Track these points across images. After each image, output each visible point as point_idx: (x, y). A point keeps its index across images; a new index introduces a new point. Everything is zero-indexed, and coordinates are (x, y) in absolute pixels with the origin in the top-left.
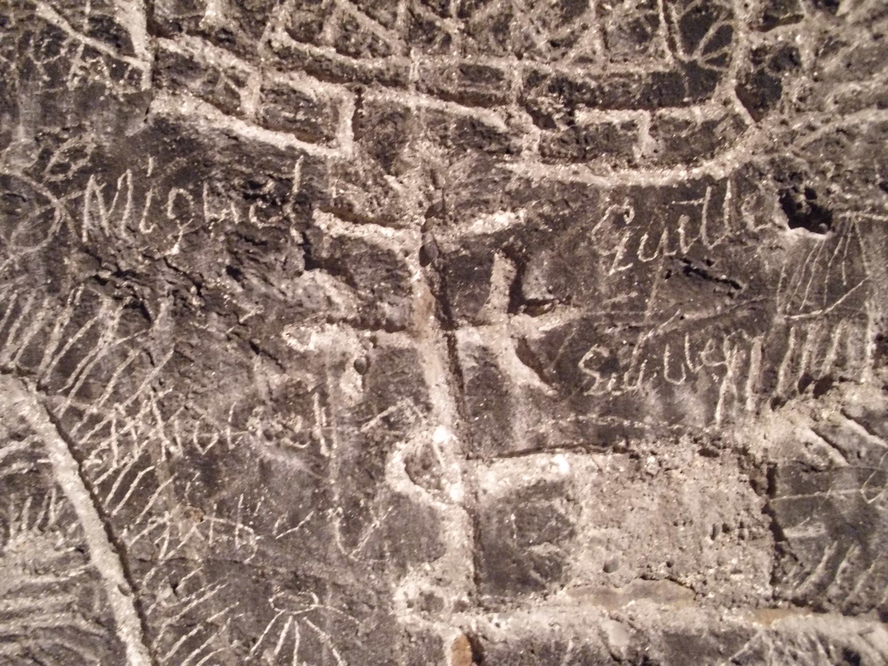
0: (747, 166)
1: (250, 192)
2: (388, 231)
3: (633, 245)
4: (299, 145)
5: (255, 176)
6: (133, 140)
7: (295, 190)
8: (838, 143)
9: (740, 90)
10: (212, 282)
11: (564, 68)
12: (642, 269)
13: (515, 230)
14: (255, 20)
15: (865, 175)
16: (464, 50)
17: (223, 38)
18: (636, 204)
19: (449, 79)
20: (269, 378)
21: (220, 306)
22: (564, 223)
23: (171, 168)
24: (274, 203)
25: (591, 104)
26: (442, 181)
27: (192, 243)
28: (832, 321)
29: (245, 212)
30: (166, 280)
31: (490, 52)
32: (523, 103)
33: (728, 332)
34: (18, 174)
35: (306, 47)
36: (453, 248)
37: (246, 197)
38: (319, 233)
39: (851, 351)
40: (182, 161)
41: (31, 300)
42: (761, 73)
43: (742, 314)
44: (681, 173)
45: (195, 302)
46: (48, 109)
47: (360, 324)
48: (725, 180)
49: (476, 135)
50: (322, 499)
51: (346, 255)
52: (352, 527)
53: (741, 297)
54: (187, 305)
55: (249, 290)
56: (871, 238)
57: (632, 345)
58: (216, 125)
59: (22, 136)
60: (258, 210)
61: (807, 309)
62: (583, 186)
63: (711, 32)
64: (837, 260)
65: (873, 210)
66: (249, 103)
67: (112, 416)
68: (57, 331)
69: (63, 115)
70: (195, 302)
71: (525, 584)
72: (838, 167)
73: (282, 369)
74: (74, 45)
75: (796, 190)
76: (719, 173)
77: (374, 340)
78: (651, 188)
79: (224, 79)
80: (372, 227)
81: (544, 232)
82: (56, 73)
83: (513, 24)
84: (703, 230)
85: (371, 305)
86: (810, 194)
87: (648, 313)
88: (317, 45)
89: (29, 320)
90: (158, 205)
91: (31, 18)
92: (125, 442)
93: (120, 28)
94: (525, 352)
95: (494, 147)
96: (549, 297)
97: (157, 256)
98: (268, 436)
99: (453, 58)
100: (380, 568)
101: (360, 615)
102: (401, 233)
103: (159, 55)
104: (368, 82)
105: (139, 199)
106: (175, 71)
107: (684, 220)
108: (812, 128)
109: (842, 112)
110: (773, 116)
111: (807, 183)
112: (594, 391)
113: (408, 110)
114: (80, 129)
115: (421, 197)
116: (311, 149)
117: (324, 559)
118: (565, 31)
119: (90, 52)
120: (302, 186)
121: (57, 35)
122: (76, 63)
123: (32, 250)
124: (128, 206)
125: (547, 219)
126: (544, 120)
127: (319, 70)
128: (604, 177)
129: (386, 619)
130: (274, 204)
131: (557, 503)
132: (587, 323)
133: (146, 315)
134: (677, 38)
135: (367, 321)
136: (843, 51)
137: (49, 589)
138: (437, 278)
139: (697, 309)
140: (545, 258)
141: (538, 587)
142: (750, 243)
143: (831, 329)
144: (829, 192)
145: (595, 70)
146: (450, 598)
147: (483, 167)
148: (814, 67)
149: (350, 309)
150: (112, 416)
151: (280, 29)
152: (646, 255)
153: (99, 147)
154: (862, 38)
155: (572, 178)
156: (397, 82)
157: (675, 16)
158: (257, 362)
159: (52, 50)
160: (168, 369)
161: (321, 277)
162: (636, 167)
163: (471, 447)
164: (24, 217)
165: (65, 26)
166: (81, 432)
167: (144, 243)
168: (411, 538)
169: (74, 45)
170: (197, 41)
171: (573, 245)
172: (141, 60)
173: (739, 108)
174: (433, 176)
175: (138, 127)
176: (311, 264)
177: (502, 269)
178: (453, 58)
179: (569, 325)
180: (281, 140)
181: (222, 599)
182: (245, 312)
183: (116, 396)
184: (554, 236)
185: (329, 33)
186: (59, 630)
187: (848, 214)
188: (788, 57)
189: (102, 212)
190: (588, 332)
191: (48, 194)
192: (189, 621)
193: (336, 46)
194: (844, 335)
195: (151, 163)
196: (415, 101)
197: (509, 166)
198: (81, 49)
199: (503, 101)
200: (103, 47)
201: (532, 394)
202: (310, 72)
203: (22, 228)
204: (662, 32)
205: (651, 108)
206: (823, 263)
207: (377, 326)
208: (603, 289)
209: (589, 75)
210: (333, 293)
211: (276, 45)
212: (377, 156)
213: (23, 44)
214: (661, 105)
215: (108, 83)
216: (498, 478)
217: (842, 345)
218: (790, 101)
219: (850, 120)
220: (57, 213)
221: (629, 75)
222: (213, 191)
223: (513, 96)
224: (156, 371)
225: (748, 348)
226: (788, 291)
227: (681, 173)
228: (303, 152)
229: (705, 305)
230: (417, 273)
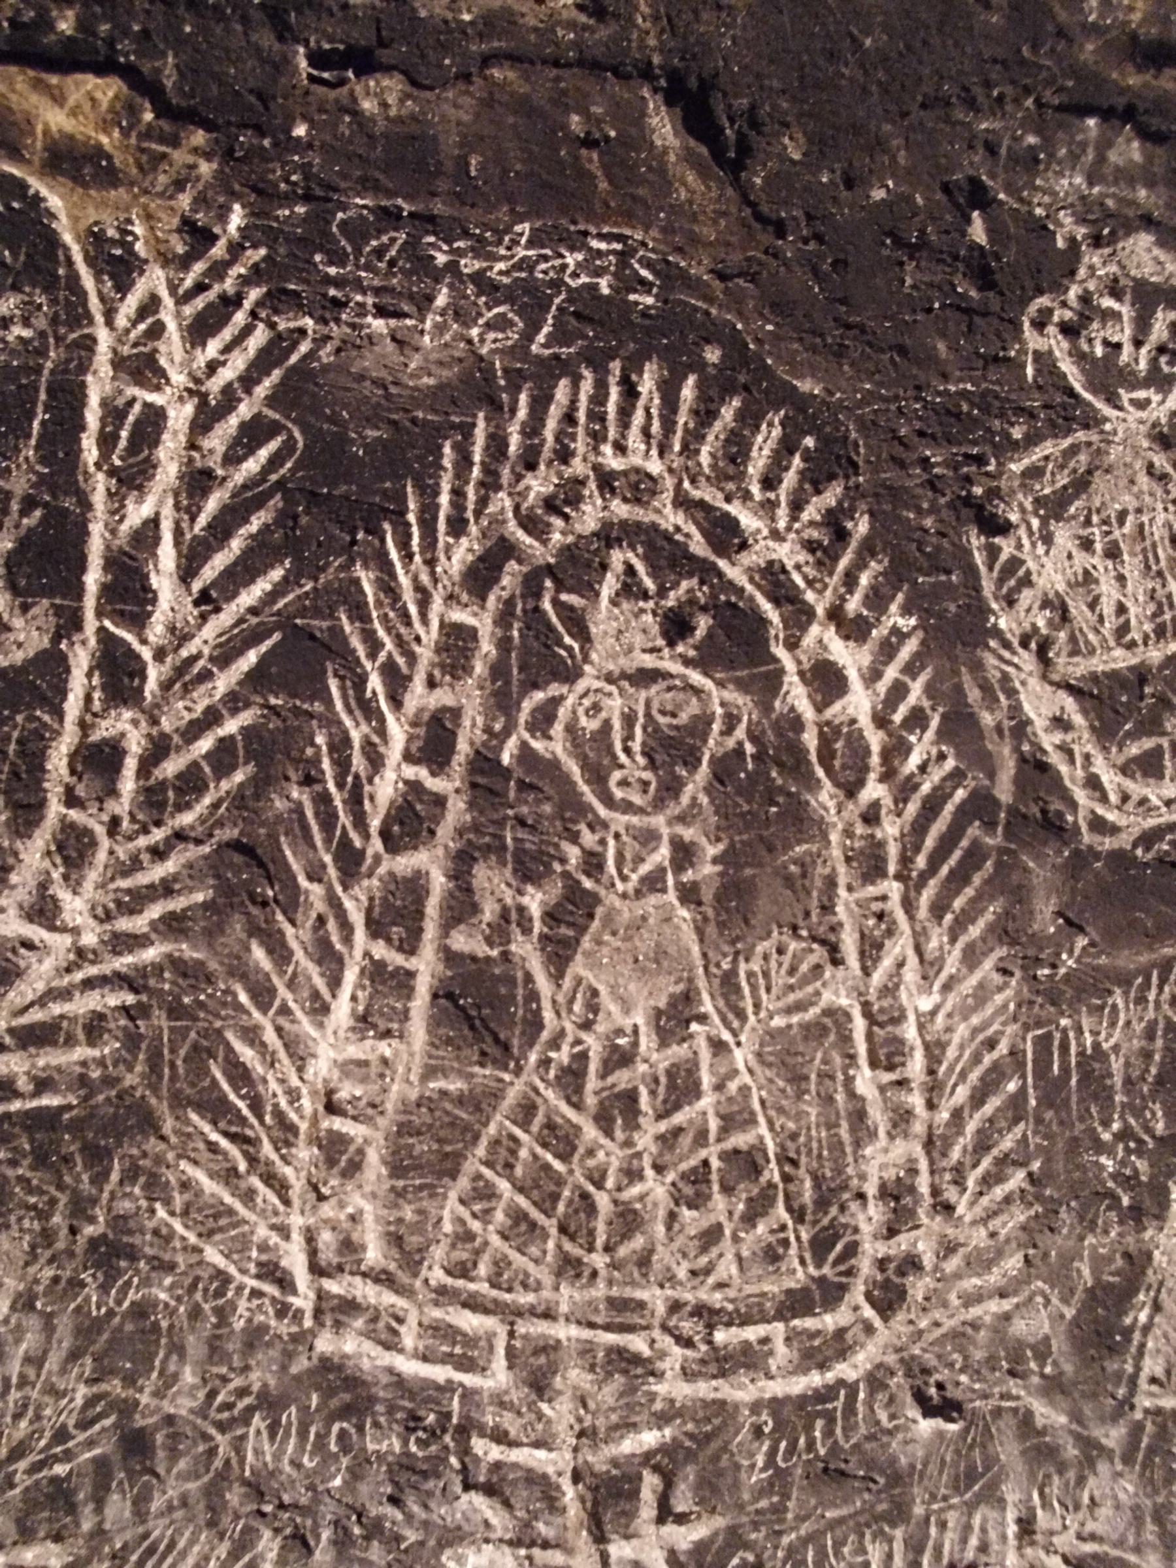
0: (879, 1366)
1: (413, 1422)
2: (541, 1454)
3: (773, 1452)
4: (458, 1376)
5: (414, 1406)
6: (297, 1378)
7: (455, 1421)
8: (964, 1335)
9: (868, 1296)
10: (374, 1511)
11: (703, 1295)
12: (780, 1474)
13: (663, 1449)
15: (991, 1362)
16: (610, 1283)
17: (384, 1278)
18: (774, 1414)
19: (596, 1310)
21: (382, 1533)
22: (709, 1437)
23: (334, 1403)
24: (433, 1433)
25: (729, 1324)
26: (592, 1405)
27: (355, 1475)
28: (970, 1508)
29: (405, 1443)
30: (328, 1511)
31: (633, 1284)
32: (665, 1328)
33: (868, 1526)
34: (184, 1412)
35: (460, 1283)
36: (604, 1468)
37: (407, 1428)
38: (477, 1460)
39: (993, 1535)
41: (187, 1534)
42: (887, 1280)
43: (882, 1507)
44: (816, 1379)
45: (357, 1531)
46: (215, 1349)
47: (515, 1543)
48: (857, 1382)
51: (503, 1479)
53: (879, 1492)
54: (346, 1531)
55: (409, 1517)
56: (1002, 1424)
57: (776, 1547)
58: (379, 1363)
59: (189, 1376)
60: (418, 1440)
61: (945, 1498)
62: (723, 1403)
63: (839, 1247)
64: (971, 1447)
65: (1002, 1397)
66: (409, 1340)
69: (229, 1356)
70: (357, 1531)
72: (966, 1358)
74: (240, 1289)
75: (926, 1384)
76: (851, 1375)
77: (529, 1558)
78: (788, 1398)
79: (385, 1319)
80: (526, 1450)
81: (688, 1449)
83: (655, 1258)
84: (839, 1431)
85: (527, 1525)
86: (940, 1386)
87: (790, 1516)
88: (472, 1280)
90: (321, 1438)
91: (200, 1263)
93: (285, 1271)
95: (639, 1371)
96: (696, 1509)
97: (320, 1488)
99: (600, 1290)
102: (553, 1455)
103: (321, 1295)
104: (520, 1314)
105: (303, 1434)
107: (819, 1424)
108: (937, 1324)
109: (966, 1305)
110: (901, 1316)
111: (937, 1377)
113: (558, 1341)
114: (246, 1369)
115: (572, 1420)
116: (469, 1380)
118: (703, 1260)
119: (256, 1293)
120: (460, 1417)
121: (224, 1279)
122: (243, 1305)
123: (192, 1486)
124: (292, 1441)
125: (690, 1436)
127: (473, 1304)
128: (742, 1391)
130: (434, 1434)
133: (305, 1544)
134: (808, 1256)
136: (962, 1251)
138: (589, 1496)
139: (836, 1506)
140: (690, 1472)
142: (885, 1439)
143: (970, 1515)
144: (958, 1384)
145: (732, 1293)
147: (631, 1390)
148: (936, 1268)
149: (506, 1529)
151: (436, 1268)
152: (785, 1460)
153: (265, 1385)
154: (979, 1237)
155: (712, 1395)
156: (548, 1315)
157: (805, 1236)
159: (220, 1293)
161: (478, 1500)
162: (772, 1378)
164: (187, 1452)
165: (232, 1270)
167: (307, 1477)
169: (240, 1289)
170: (358, 1280)
171: (716, 1458)
172: (303, 1301)
173: (868, 1312)
175: (300, 1365)
176: (467, 1487)
177: (650, 1483)
178: (600, 1290)
179: (716, 1534)
180: (440, 1373)
182: (405, 1539)
184: (699, 1453)
185: (483, 1270)
187: (977, 1403)
188: (912, 1263)
189: (266, 1447)
191: (212, 1431)
193: (490, 1281)
194: (985, 1520)
195: (315, 1399)
196: (564, 1332)
197: (654, 1388)
198: (247, 1291)
199: (647, 1328)
202: (465, 1305)
203: (182, 1464)
204: (793, 1251)
205: (786, 1320)
206: (958, 1452)
207: (532, 1544)
208: (746, 1496)
209: (727, 1299)
210: (489, 1514)
211: (433, 1283)
212: (531, 1386)
213: (193, 1287)
214: (794, 1317)
215: (273, 1323)
217: (984, 1530)
219: (975, 1311)
220: (221, 1450)
221: (763, 1295)
222: (376, 1425)
223: (656, 1322)
225: (890, 1541)
226: (926, 1482)
227: (816, 1379)
228: (461, 1385)
229: (846, 1501)
230: (569, 1493)
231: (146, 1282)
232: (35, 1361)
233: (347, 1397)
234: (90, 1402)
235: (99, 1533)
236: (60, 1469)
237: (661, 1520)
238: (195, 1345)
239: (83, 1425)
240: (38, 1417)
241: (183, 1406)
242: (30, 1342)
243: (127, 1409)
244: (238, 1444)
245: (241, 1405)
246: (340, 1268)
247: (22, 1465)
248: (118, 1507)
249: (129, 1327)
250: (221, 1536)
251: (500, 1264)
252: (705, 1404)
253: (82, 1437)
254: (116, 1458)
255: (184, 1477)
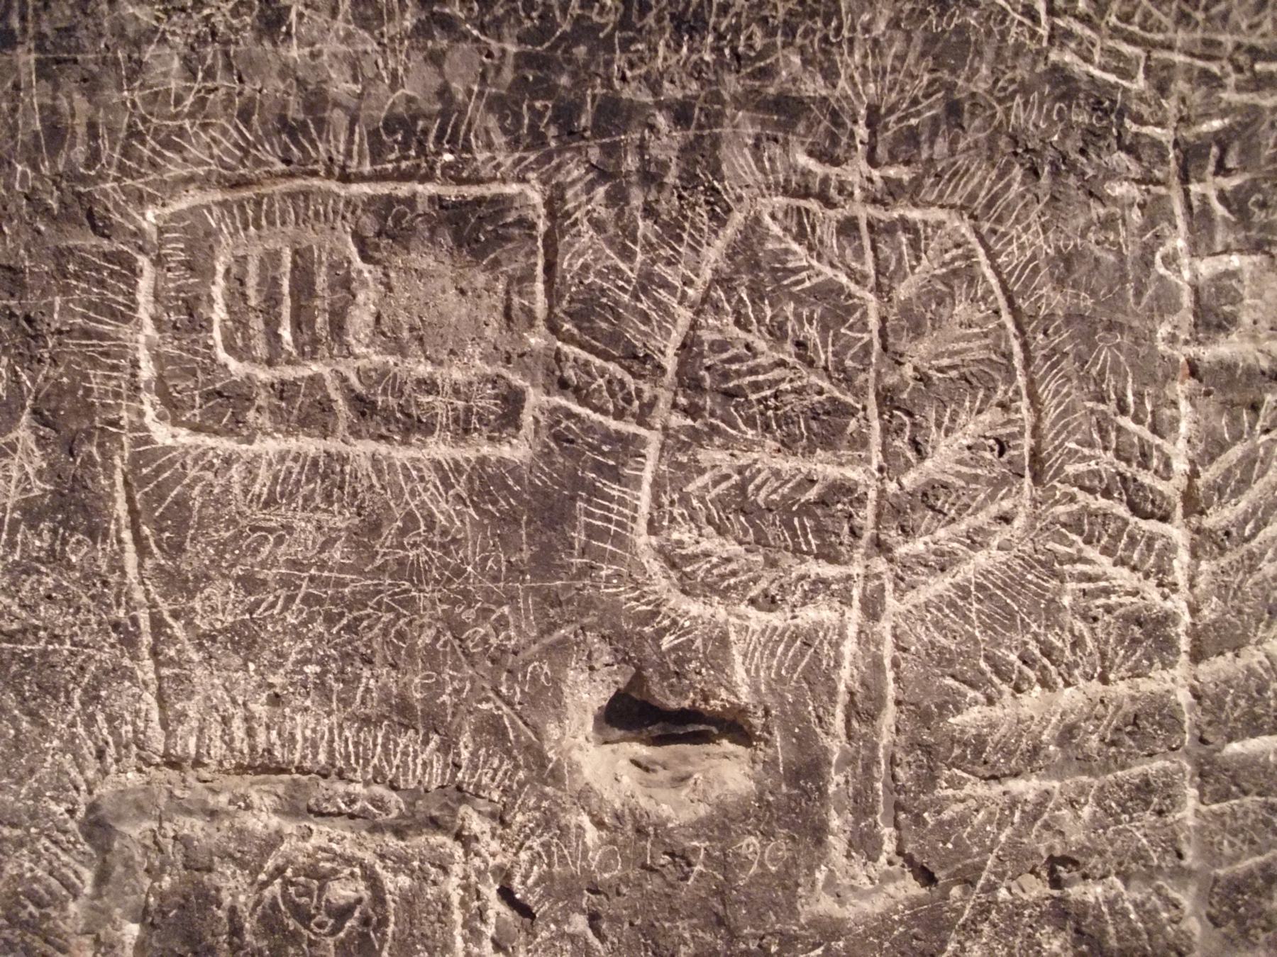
2: (1158, 130)
6: (1040, 75)
14: (1102, 11)
16: (1205, 30)
17: (1085, 19)
20: (1099, 211)
23: (1057, 92)
27: (1065, 135)
30: (1050, 153)
31: (1217, 30)
32: (1231, 60)
35: (1123, 26)
40: (1064, 88)
47: (1138, 182)
49: (1207, 78)
50: (1124, 278)
52: (1139, 294)
54: (1058, 168)
59: (984, 71)
67: (1014, 233)
68: (988, 183)
71: (1220, 327)
73: (1104, 206)
79: (1086, 44)
82: (1004, 35)
85: (1150, 171)
89: (973, 175)
90: (1050, 111)
92: (1022, 247)
94: (1222, 197)
98: (1097, 243)
99: (1198, 34)
100: (1151, 318)
101: (1140, 345)
103: (1053, 27)
106: (1059, 37)
112: (1255, 219)
114: (1014, 68)
116: (1125, 83)
117: (1125, 313)
118: (1256, 19)
119: (1021, 24)
122: (1014, 30)
123: (982, 135)
125: (1239, 124)
126: (1239, 69)
127: (1131, 39)
129: (1153, 348)
130: (1106, 113)
131: (1234, 282)
132: (1254, 180)
135: (1146, 180)
137: (976, 335)
141: (1225, 329)
146: (1183, 336)
150: (1014, 233)
156: (1169, 47)
158: (1091, 201)
159: (1003, 22)
160: (1047, 204)
161: (1123, 155)
163: (1194, 250)
166: (996, 242)
168: (1165, 303)
171: (1250, 138)
172: (1044, 31)
174: (1183, 100)
175: (1041, 68)
178: (1198, 34)
180: (1112, 78)
181: (1072, 337)
183: (1017, 221)
185: (1137, 19)
186: (980, 361)
190: (1254, 186)
192: (1054, 351)
196: (1179, 58)
199: (1220, 59)
200: (1027, 22)
201: (1225, 219)
203: (977, 122)
216: (1207, 267)
218: (159, 262)
222: (1078, 106)
224: (1041, 206)
231: (963, 13)
232: (901, 58)
233: (1064, 88)
234: (931, 83)
235: (930, 160)
236: (913, 121)
237: (1216, 174)
238: (989, 54)
239: (927, 96)
240: (902, 90)
241: (981, 87)
242: (897, 47)
243: (951, 88)
244: (1007, 111)
245: (1011, 89)
246: (1065, 12)
247: (893, 118)
248: (941, 146)
249: (954, 39)
250: (993, 166)
251: (1147, 15)
252: (1246, 105)
253: (925, 103)
254: (943, 116)
255: (978, 130)
